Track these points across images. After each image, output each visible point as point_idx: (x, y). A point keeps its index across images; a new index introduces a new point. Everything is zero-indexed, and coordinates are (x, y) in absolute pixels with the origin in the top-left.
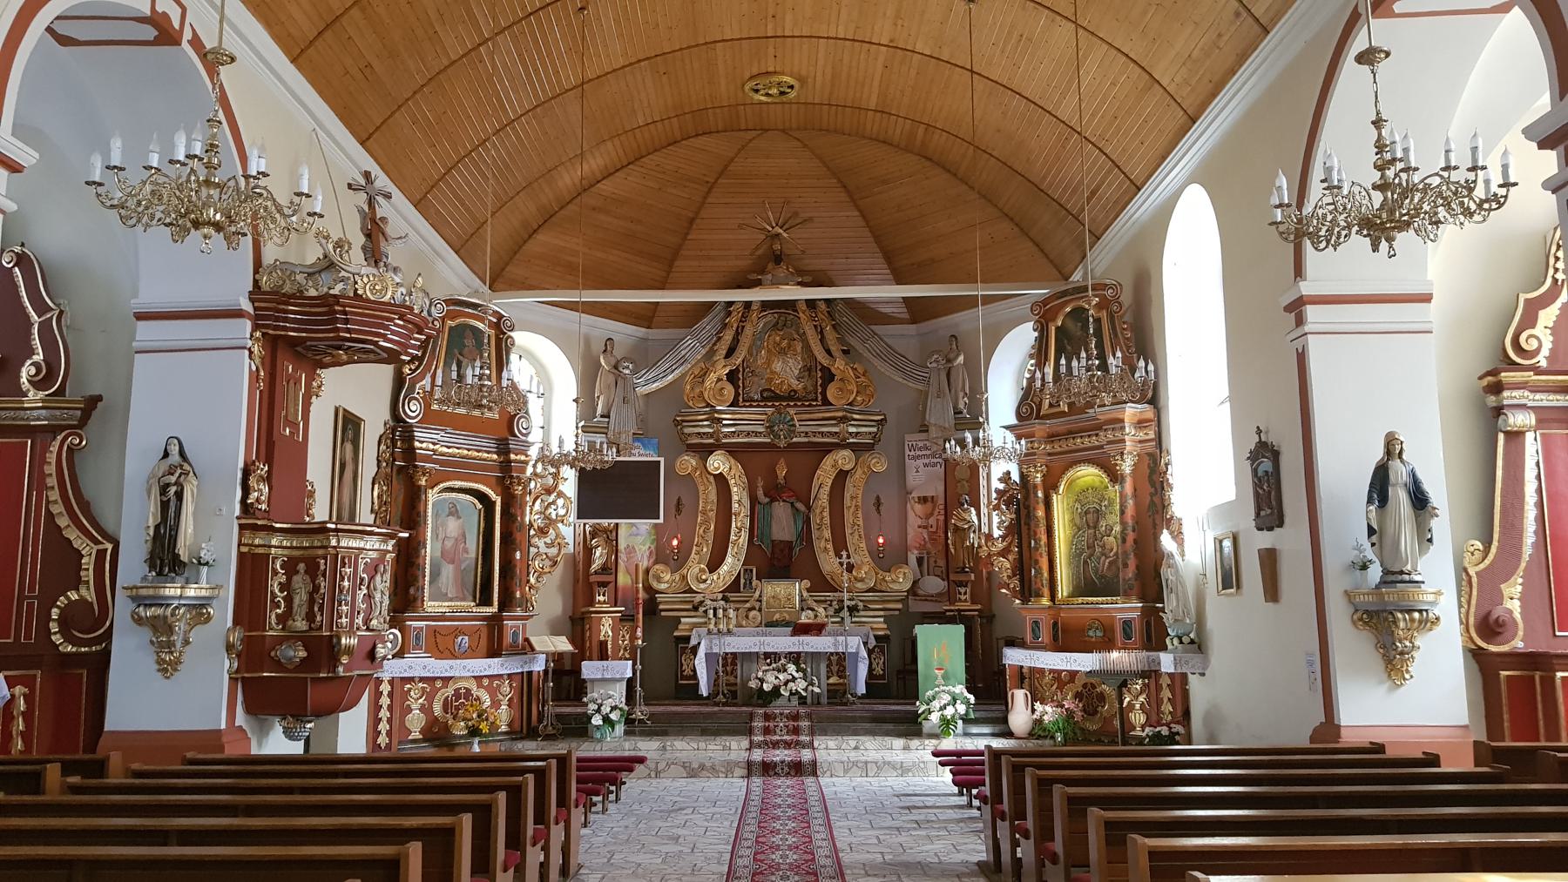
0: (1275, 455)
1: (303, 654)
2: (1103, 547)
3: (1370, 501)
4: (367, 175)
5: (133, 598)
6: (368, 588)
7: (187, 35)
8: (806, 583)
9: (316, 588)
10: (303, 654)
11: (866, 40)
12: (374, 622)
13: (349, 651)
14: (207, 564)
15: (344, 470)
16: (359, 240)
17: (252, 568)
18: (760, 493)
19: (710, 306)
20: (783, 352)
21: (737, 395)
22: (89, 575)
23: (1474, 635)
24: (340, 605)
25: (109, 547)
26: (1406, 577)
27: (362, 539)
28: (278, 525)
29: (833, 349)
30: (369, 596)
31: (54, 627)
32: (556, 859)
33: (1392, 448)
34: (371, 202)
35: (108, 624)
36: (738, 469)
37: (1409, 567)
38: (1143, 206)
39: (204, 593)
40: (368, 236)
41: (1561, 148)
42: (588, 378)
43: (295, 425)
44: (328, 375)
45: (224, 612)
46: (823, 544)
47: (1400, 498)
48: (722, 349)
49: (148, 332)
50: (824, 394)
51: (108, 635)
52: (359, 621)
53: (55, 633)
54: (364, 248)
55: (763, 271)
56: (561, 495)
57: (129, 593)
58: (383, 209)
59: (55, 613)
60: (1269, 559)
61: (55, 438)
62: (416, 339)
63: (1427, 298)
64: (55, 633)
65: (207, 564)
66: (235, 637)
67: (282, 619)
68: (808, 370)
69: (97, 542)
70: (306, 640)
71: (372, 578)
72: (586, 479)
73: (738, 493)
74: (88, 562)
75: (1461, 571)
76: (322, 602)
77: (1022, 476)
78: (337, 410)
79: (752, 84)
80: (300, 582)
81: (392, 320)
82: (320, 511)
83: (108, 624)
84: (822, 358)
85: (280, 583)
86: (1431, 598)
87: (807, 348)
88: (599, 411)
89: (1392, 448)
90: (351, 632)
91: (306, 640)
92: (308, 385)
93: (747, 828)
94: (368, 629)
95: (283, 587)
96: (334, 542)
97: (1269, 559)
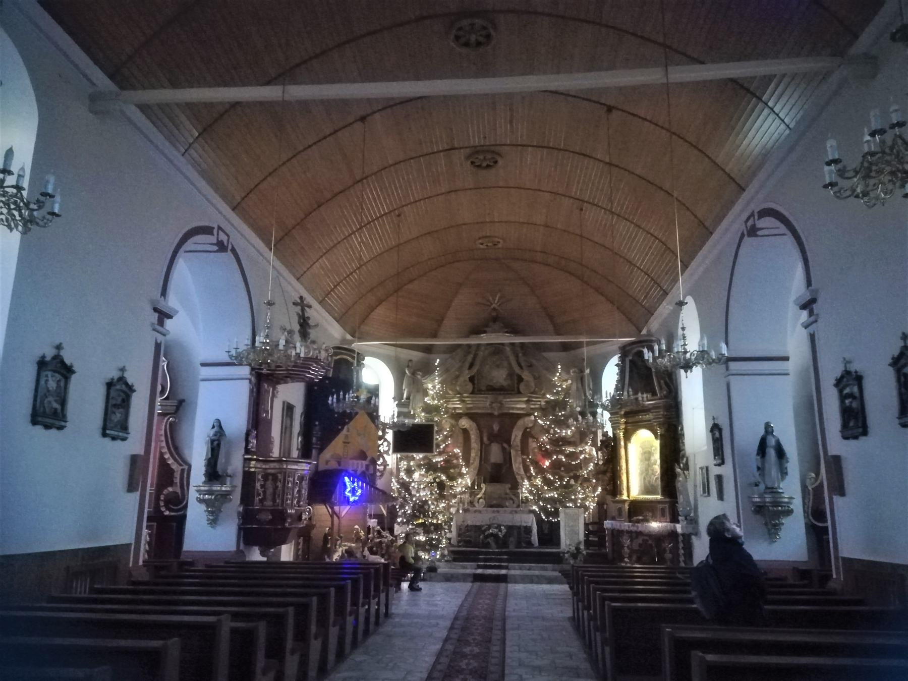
0: (720, 430)
1: (270, 517)
2: (653, 470)
3: (758, 454)
4: (301, 298)
5: (198, 491)
6: (299, 487)
7: (230, 247)
8: (509, 486)
9: (277, 487)
10: (270, 517)
11: (594, 99)
12: (301, 503)
13: (291, 515)
14: (230, 476)
15: (286, 429)
16: (297, 327)
17: (248, 477)
18: (485, 439)
19: (459, 346)
20: (498, 366)
21: (474, 388)
22: (177, 480)
23: (811, 518)
24: (287, 495)
25: (186, 467)
26: (775, 490)
27: (297, 465)
28: (261, 459)
29: (523, 364)
30: (299, 492)
31: (162, 504)
32: (383, 610)
33: (769, 430)
34: (303, 310)
35: (185, 502)
36: (474, 425)
37: (776, 485)
38: (665, 308)
39: (228, 489)
40: (301, 325)
41: (808, 310)
42: (399, 377)
43: (267, 412)
44: (281, 388)
45: (237, 497)
46: (517, 465)
47: (771, 453)
48: (467, 365)
49: (205, 372)
50: (518, 389)
51: (186, 507)
52: (295, 502)
53: (162, 506)
54: (299, 331)
55: (487, 326)
56: (386, 440)
57: (196, 488)
58: (309, 313)
59: (162, 497)
60: (719, 478)
61: (164, 419)
62: (321, 372)
63: (786, 359)
64: (162, 506)
65: (230, 476)
66: (241, 509)
67: (261, 501)
68: (511, 374)
69: (181, 465)
70: (273, 512)
71: (301, 483)
72: (398, 435)
73: (474, 436)
74: (177, 475)
75: (804, 488)
76: (279, 494)
77: (614, 434)
78: (284, 403)
79: (480, 241)
80: (269, 484)
81: (311, 365)
82: (276, 453)
83: (185, 502)
84: (517, 370)
85: (261, 485)
86: (786, 500)
87: (510, 364)
88: (405, 396)
89: (769, 430)
90: (292, 507)
91: (273, 512)
92: (273, 393)
93: (499, 637)
94: (299, 506)
95: (262, 486)
96: (285, 467)
97: (719, 478)
